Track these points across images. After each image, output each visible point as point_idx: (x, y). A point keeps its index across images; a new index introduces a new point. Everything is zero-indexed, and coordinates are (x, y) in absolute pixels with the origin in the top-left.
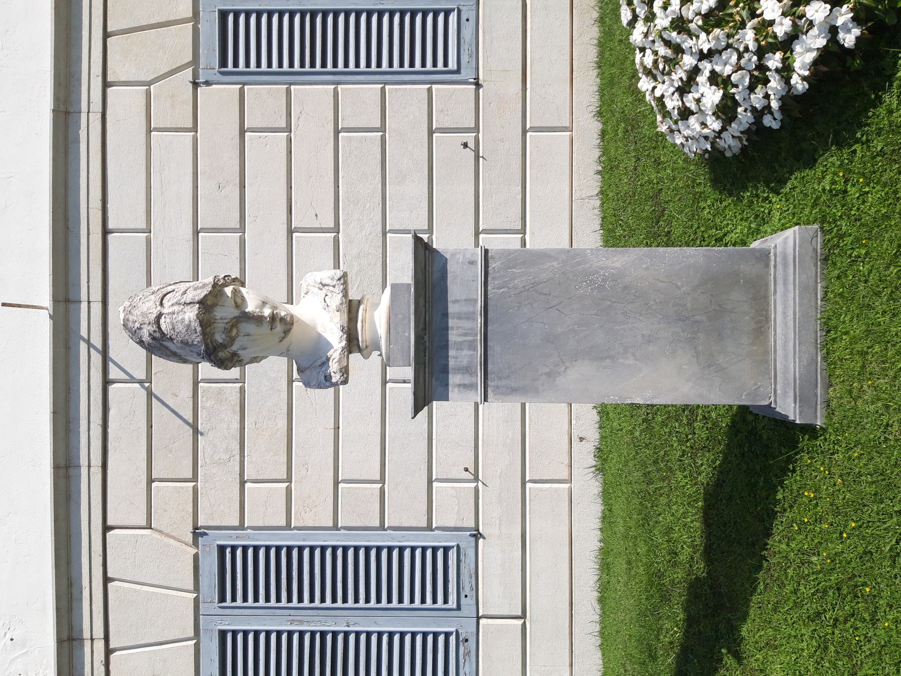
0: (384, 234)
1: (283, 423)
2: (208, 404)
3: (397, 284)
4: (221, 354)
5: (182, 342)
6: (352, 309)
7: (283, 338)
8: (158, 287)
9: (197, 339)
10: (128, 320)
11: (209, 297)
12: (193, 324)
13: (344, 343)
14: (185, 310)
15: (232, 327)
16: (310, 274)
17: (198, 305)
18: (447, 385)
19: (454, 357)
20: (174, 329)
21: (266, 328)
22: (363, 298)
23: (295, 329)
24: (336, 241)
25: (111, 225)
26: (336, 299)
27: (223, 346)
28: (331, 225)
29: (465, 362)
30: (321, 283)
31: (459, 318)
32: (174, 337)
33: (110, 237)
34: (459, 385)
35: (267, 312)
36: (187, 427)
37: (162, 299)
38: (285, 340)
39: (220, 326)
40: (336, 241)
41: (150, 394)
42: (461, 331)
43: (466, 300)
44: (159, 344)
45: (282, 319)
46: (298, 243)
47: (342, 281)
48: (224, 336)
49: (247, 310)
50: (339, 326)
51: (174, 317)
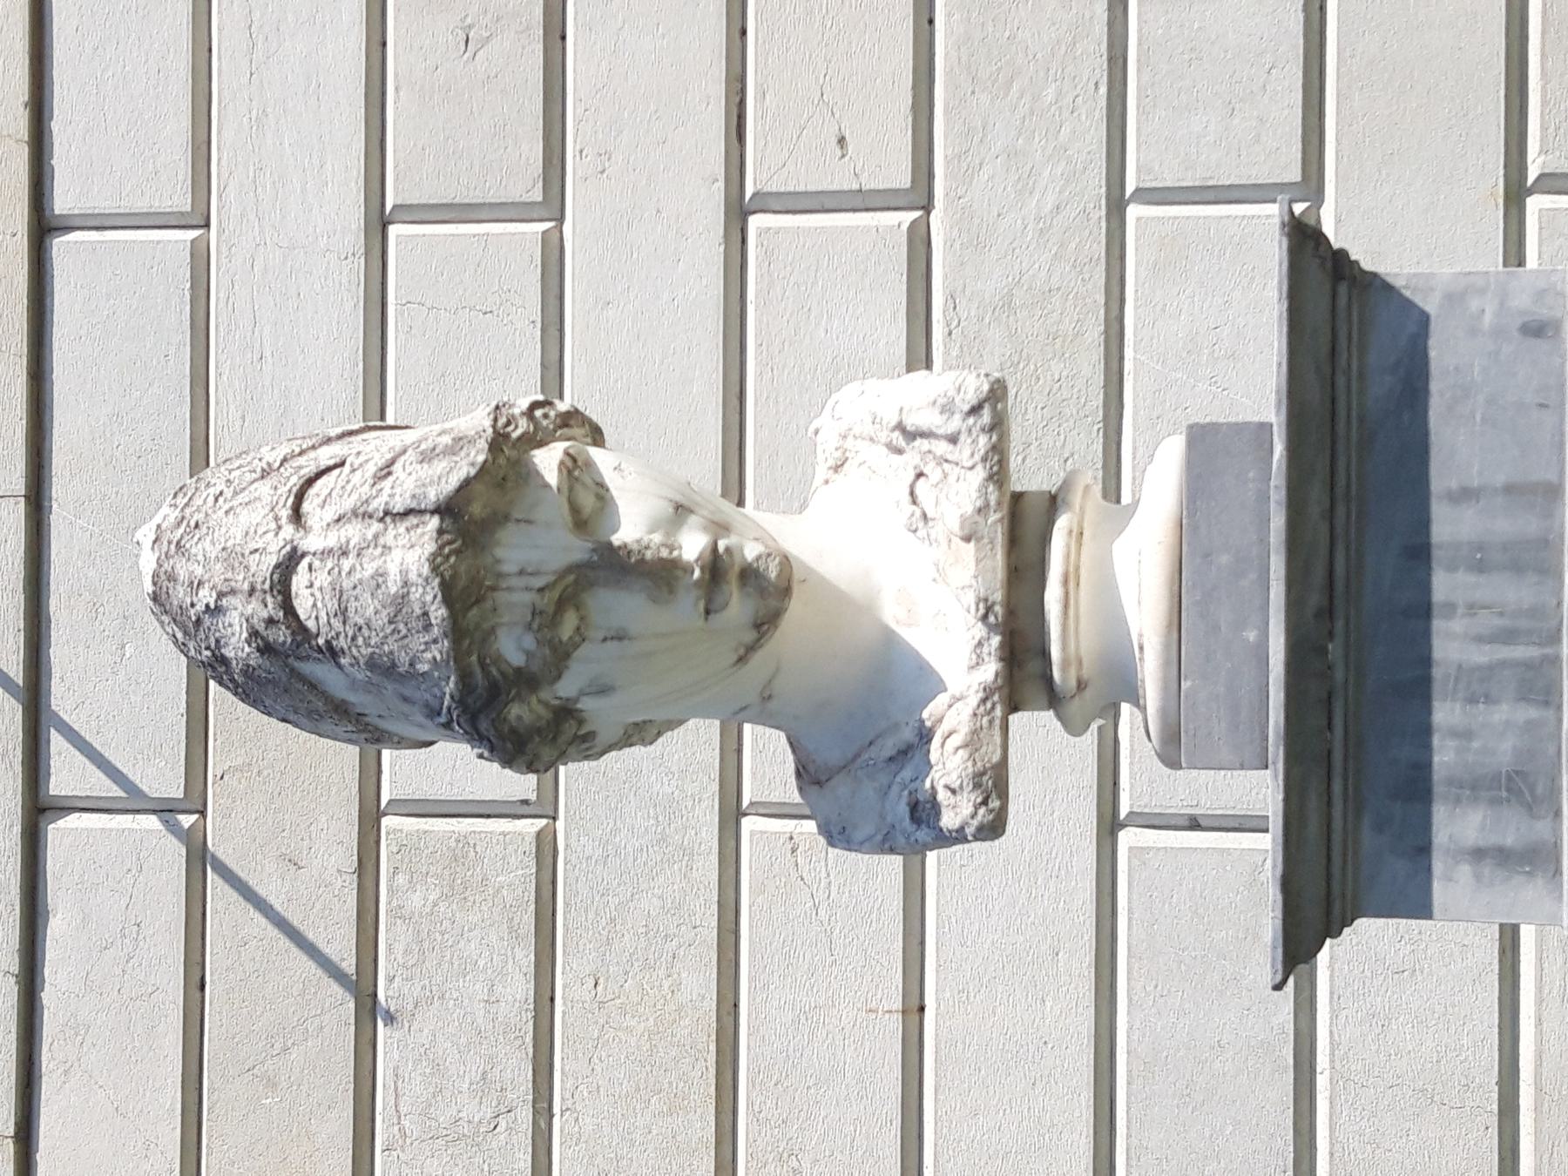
0: (1116, 206)
1: (700, 984)
2: (416, 900)
3: (1213, 428)
4: (517, 712)
5: (372, 663)
6: (1023, 530)
7: (751, 648)
8: (284, 450)
9: (429, 651)
10: (172, 578)
11: (479, 487)
12: (416, 593)
13: (990, 670)
14: (389, 538)
15: (561, 605)
16: (851, 389)
17: (434, 522)
18: (1422, 851)
19: (1455, 733)
20: (343, 612)
21: (687, 606)
22: (1066, 485)
23: (796, 609)
24: (919, 244)
25: (63, 202)
26: (961, 490)
27: (526, 681)
28: (901, 177)
29: (1504, 753)
30: (900, 427)
31: (1480, 567)
32: (342, 643)
33: (60, 245)
34: (1478, 854)
35: (692, 545)
36: (336, 989)
37: (300, 497)
38: (757, 659)
39: (516, 600)
40: (919, 244)
41: (199, 858)
42: (1488, 622)
43: (1509, 489)
44: (285, 670)
45: (750, 575)
46: (767, 255)
47: (986, 417)
48: (529, 642)
49: (617, 539)
50: (970, 598)
51: (346, 564)
